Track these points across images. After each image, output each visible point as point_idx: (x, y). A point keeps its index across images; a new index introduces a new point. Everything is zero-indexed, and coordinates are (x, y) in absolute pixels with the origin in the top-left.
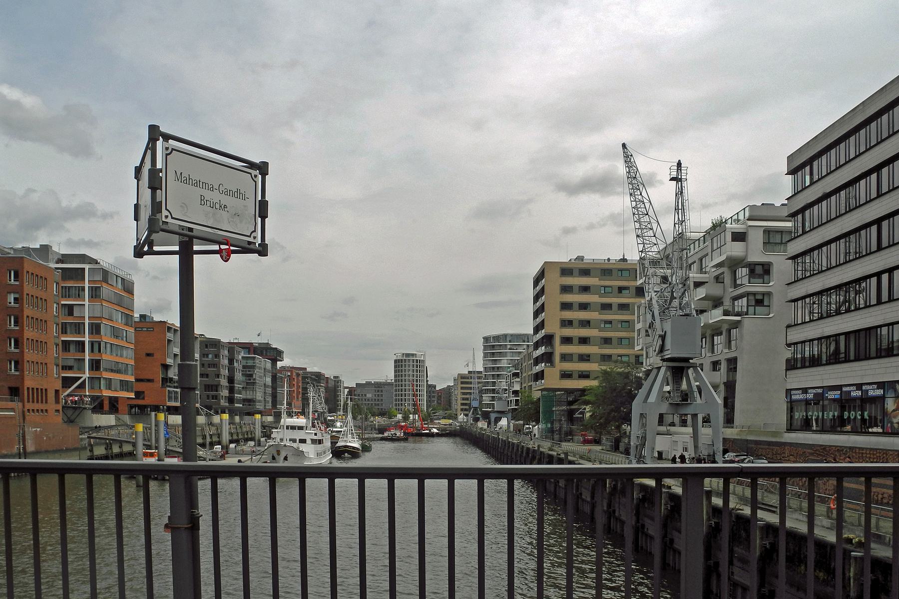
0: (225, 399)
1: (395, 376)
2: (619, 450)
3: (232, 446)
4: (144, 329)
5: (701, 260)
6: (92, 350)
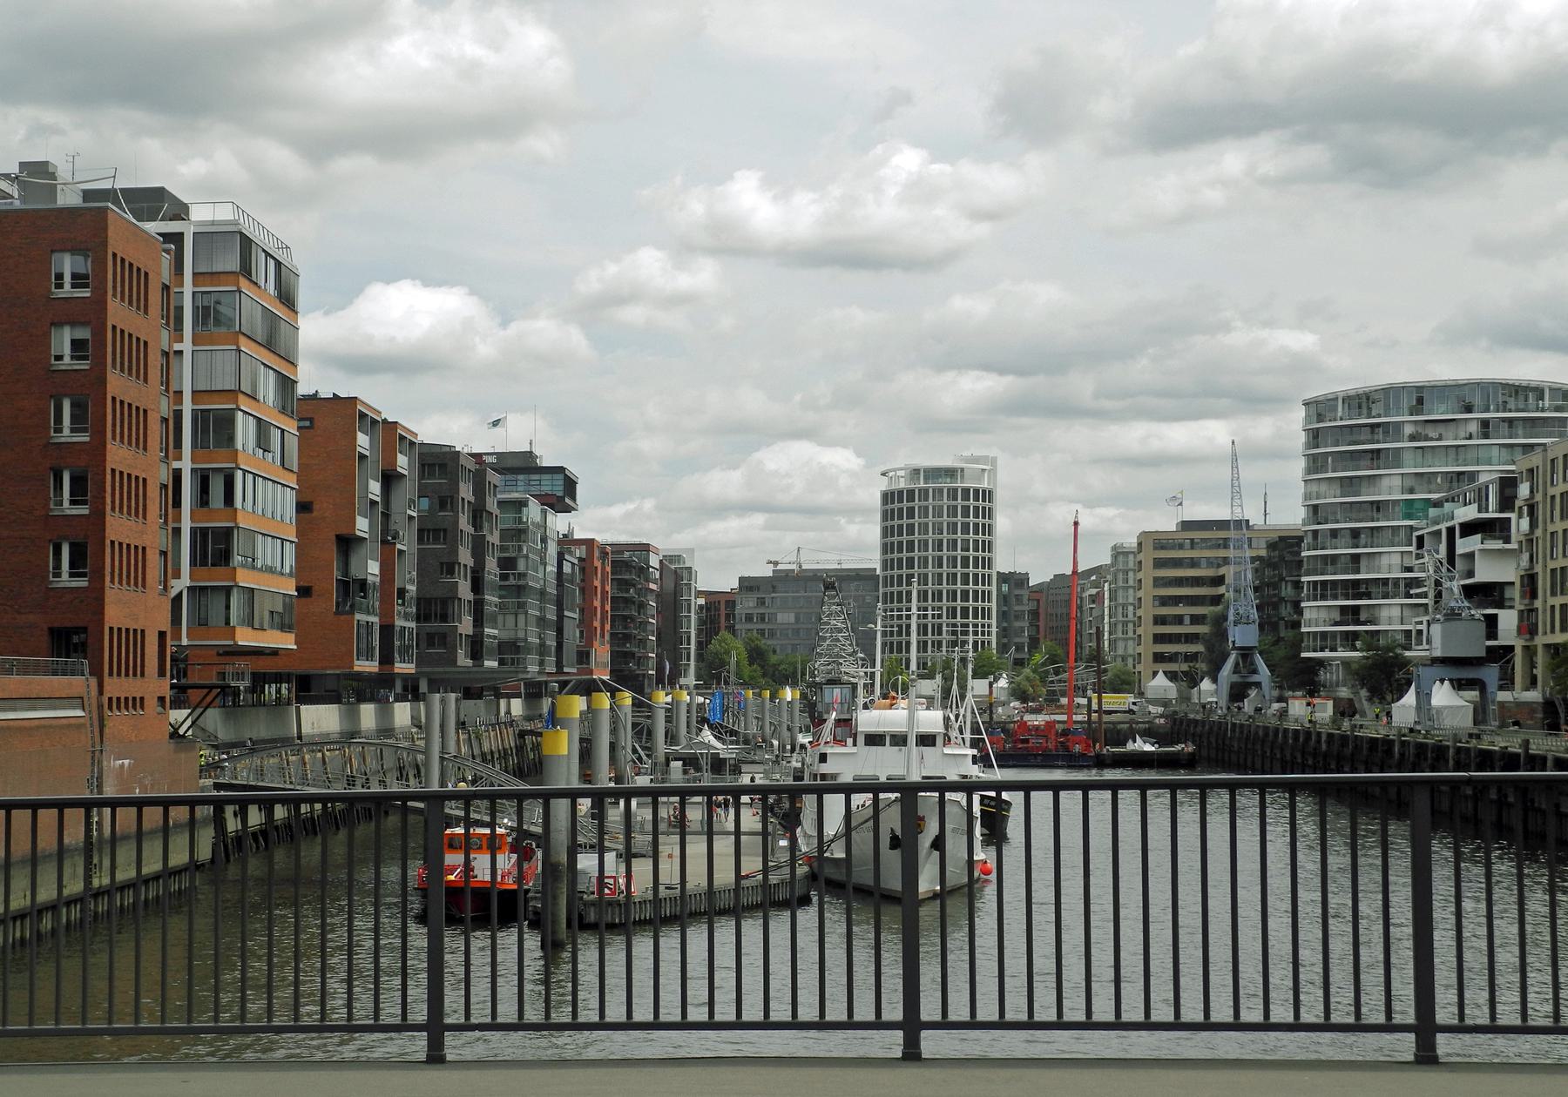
1: (886, 548)
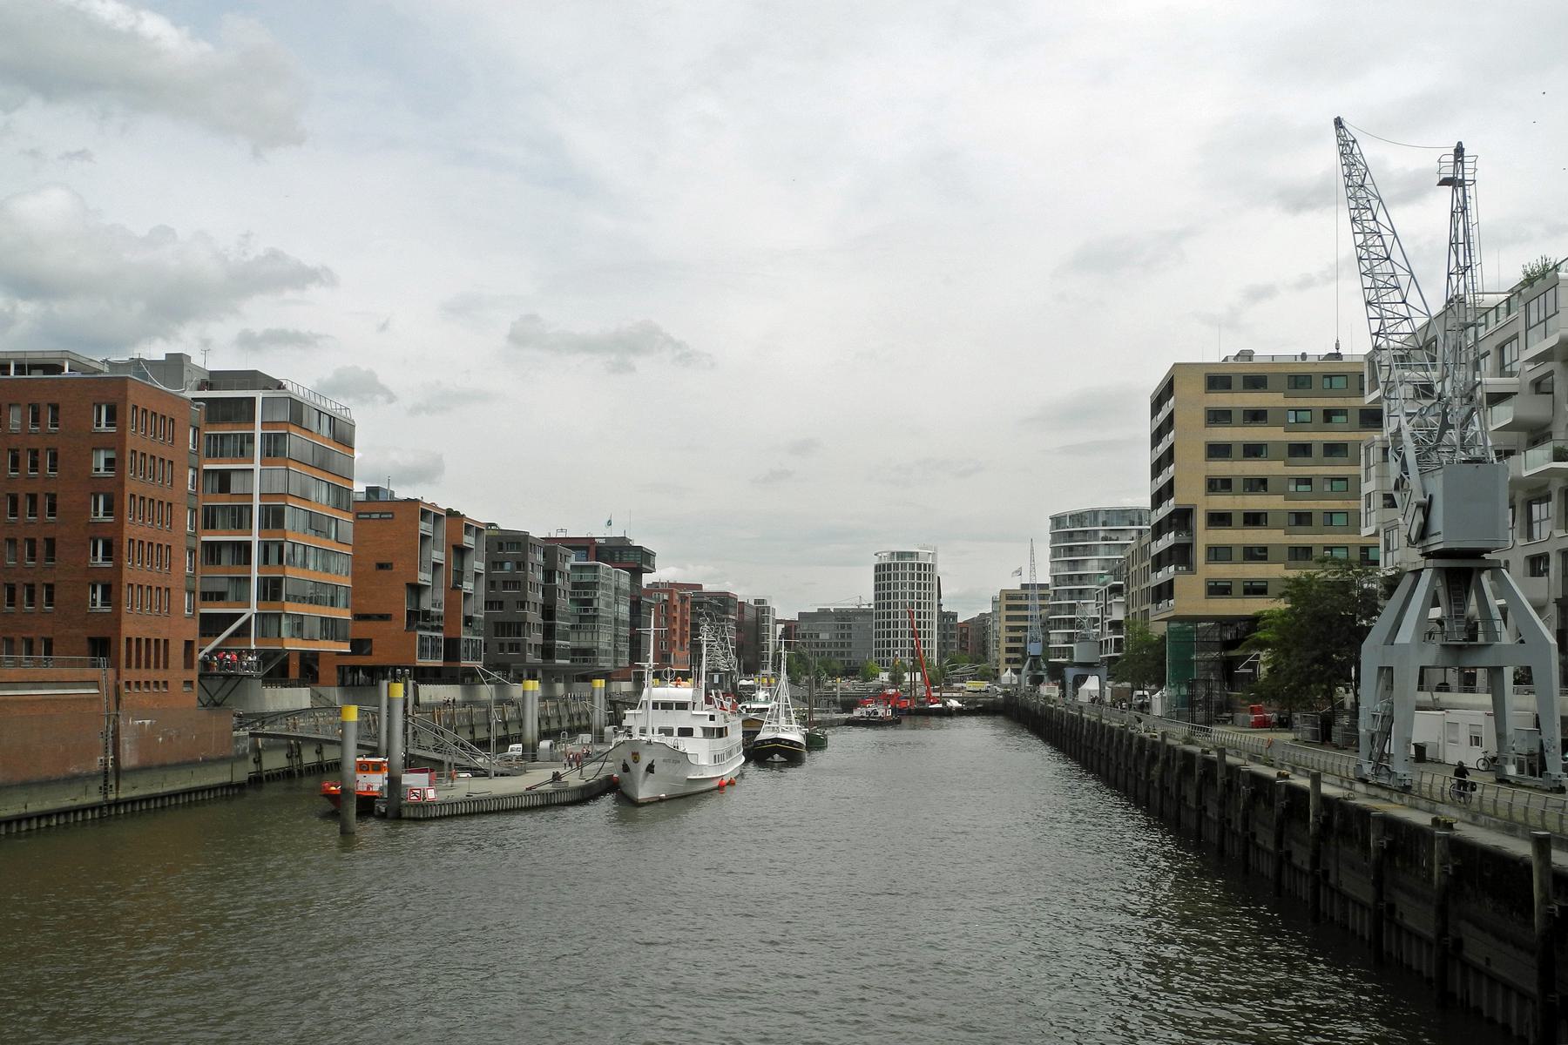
0: (535, 650)
1: (877, 597)
2: (1330, 740)
3: (545, 744)
4: (374, 516)
5: (1501, 348)
6: (265, 559)
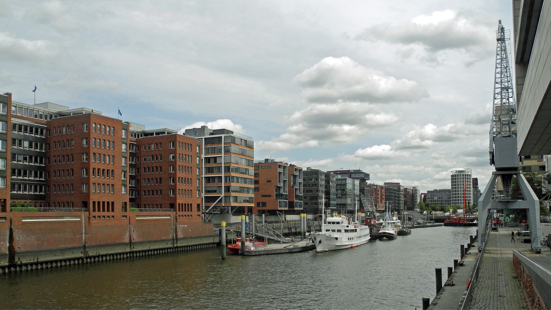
1: (452, 185)
4: (266, 167)
